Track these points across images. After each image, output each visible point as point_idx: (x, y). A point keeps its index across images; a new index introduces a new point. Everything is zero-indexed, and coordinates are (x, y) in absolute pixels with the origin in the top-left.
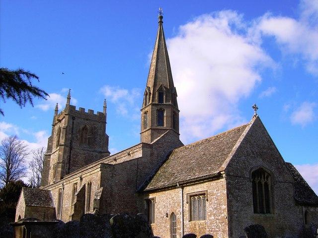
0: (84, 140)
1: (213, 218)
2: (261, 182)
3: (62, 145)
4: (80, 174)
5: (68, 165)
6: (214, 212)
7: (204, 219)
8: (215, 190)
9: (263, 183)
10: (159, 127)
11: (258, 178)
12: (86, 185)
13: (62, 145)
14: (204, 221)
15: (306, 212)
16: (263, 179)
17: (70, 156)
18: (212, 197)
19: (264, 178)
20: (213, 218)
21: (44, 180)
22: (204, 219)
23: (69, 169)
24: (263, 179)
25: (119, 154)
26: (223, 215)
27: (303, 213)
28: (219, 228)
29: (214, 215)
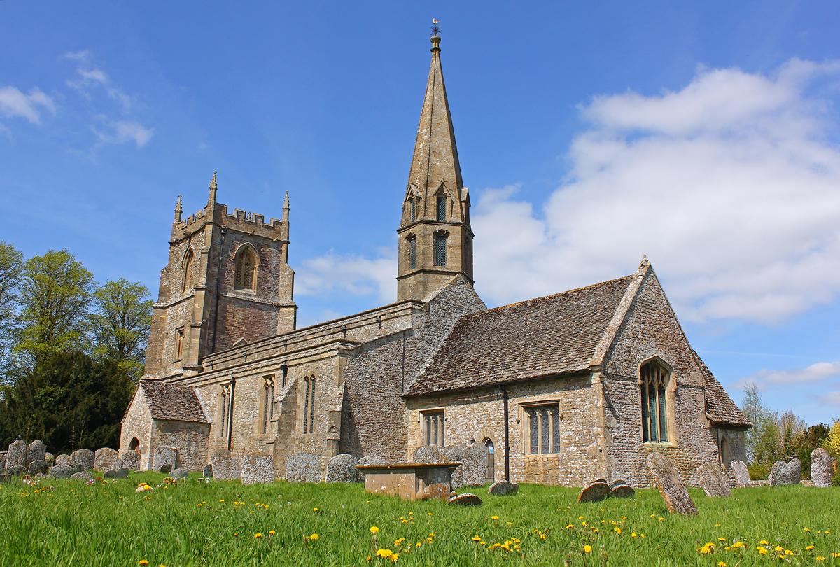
0: (243, 277)
1: (573, 448)
2: (653, 386)
3: (202, 289)
4: (283, 359)
5: (212, 332)
6: (577, 439)
7: (556, 449)
8: (579, 399)
9: (656, 387)
10: (439, 268)
11: (649, 378)
12: (301, 381)
13: (202, 289)
14: (555, 455)
15: (723, 440)
16: (656, 380)
17: (216, 313)
18: (572, 411)
19: (658, 379)
20: (573, 448)
21: (711, 421)
22: (556, 449)
23: (214, 340)
24: (656, 380)
25: (355, 320)
26: (595, 444)
27: (718, 441)
28: (587, 468)
29: (577, 444)
